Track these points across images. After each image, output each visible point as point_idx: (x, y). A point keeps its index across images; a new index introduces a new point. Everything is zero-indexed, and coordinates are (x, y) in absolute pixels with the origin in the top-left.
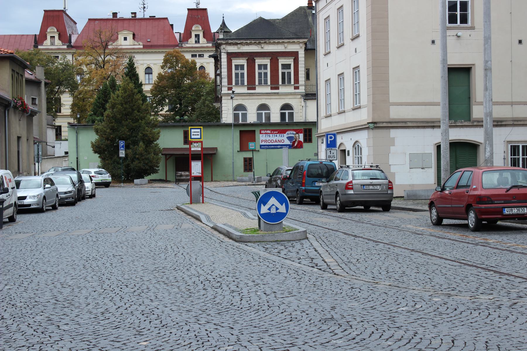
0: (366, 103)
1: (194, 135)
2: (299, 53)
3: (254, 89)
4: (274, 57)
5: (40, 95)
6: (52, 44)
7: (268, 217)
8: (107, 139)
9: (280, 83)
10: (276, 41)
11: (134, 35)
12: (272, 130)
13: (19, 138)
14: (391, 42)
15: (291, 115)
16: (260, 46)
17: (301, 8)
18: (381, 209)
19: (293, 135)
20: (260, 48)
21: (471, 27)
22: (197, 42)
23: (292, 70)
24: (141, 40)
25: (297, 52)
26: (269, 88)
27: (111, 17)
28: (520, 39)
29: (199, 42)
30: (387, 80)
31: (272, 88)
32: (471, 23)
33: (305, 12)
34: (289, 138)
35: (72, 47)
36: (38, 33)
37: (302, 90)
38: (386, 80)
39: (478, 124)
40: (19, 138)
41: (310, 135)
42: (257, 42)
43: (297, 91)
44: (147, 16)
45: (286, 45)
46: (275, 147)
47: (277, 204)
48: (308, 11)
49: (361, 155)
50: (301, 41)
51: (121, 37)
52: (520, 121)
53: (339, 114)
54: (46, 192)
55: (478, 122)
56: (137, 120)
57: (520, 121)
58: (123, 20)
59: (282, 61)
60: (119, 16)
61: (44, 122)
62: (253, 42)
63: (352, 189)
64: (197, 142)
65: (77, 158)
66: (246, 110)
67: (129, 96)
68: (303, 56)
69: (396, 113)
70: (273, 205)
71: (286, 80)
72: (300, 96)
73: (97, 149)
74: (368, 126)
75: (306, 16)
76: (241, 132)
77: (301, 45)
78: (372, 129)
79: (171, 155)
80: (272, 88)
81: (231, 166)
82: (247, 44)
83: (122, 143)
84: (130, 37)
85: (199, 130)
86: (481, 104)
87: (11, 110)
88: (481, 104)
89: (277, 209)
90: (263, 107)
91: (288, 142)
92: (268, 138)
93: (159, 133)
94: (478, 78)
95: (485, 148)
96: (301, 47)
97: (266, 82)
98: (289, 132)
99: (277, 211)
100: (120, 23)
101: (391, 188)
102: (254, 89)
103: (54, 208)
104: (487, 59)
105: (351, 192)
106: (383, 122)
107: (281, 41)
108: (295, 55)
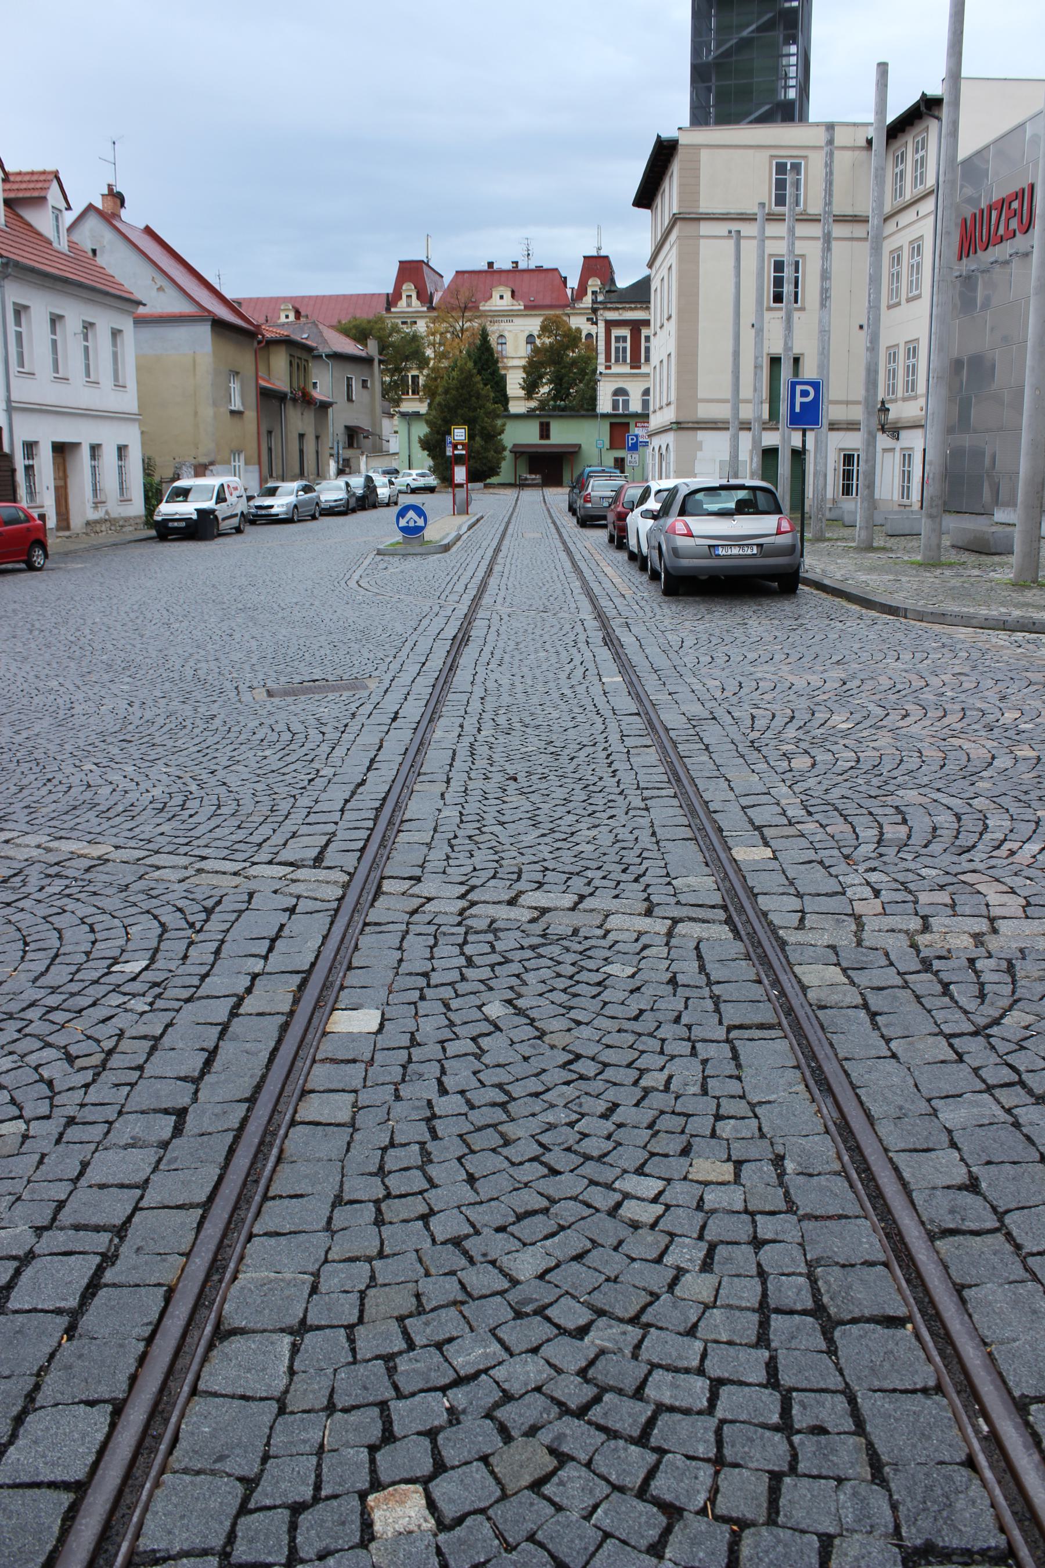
3: (639, 368)
5: (372, 375)
6: (409, 304)
7: (405, 530)
8: (438, 433)
11: (513, 292)
13: (301, 436)
14: (702, 325)
18: (170, 524)
24: (522, 299)
27: (486, 268)
35: (434, 309)
36: (390, 290)
38: (694, 372)
40: (301, 436)
44: (532, 266)
51: (496, 295)
54: (299, 501)
56: (475, 409)
58: (501, 272)
60: (496, 266)
61: (378, 410)
67: (466, 378)
73: (426, 444)
79: (523, 453)
82: (631, 309)
84: (508, 295)
87: (289, 405)
90: (620, 392)
93: (504, 425)
97: (625, 360)
100: (496, 276)
102: (639, 368)
103: (314, 518)
105: (589, 505)
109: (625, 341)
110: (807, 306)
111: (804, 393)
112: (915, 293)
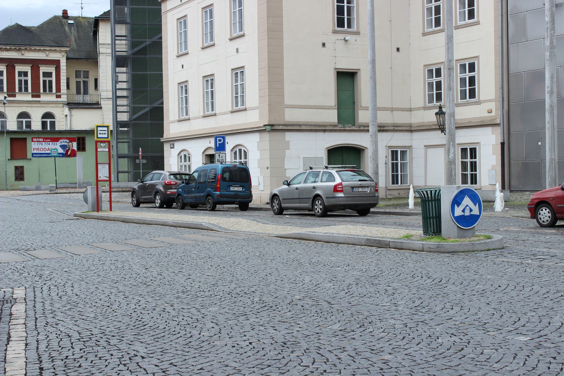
0: (256, 104)
1: (100, 134)
2: (61, 61)
4: (35, 64)
9: (42, 91)
10: (38, 48)
12: (44, 138)
14: (285, 42)
15: (53, 124)
16: (20, 53)
17: (56, 17)
19: (65, 144)
20: (20, 55)
21: (357, 32)
23: (54, 79)
25: (59, 61)
26: (30, 95)
28: (398, 47)
30: (282, 82)
31: (33, 96)
32: (357, 28)
33: (61, 22)
34: (63, 147)
37: (64, 98)
38: (281, 82)
39: (364, 129)
41: (84, 144)
42: (18, 48)
43: (59, 99)
45: (47, 53)
46: (48, 155)
47: (471, 204)
48: (64, 20)
50: (63, 49)
52: (400, 126)
53: (203, 117)
55: (364, 126)
57: (400, 126)
59: (43, 69)
62: (13, 48)
63: (341, 191)
64: (104, 142)
66: (30, 118)
68: (65, 64)
69: (291, 116)
70: (467, 206)
71: (48, 88)
72: (61, 105)
74: (264, 128)
75: (62, 25)
76: (12, 140)
77: (63, 54)
78: (269, 132)
80: (33, 96)
81: (4, 175)
82: (7, 50)
85: (99, 136)
86: (367, 109)
88: (367, 109)
89: (471, 210)
90: (23, 115)
91: (61, 151)
92: (40, 147)
94: (364, 84)
95: (449, 150)
96: (63, 56)
97: (26, 89)
98: (62, 140)
99: (472, 213)
101: (377, 191)
104: (450, 58)
105: (341, 195)
106: (279, 125)
107: (42, 48)
108: (56, 63)
109: (26, 74)
110: (361, 31)
111: (220, 140)
112: (184, 51)
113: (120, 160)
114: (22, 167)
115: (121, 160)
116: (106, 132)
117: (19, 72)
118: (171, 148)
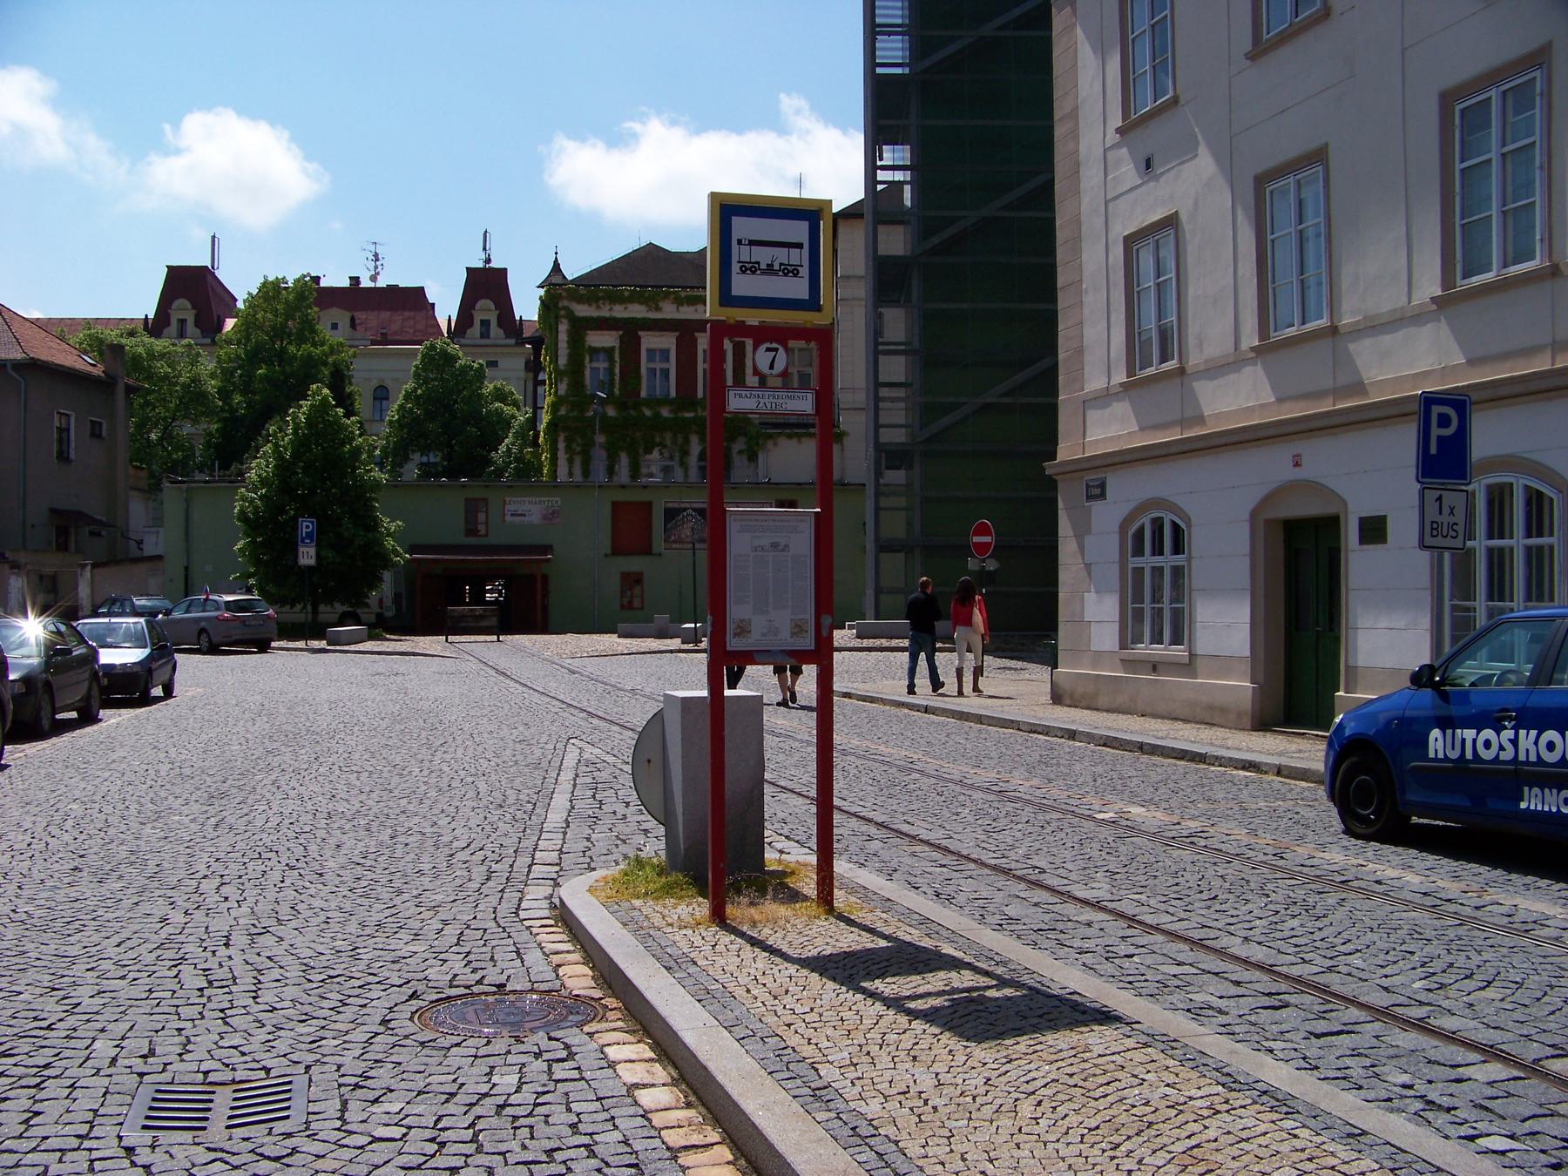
1: (750, 268)
22: (485, 334)
29: (488, 337)
49: (1178, 549)
65: (186, 568)
83: (306, 526)
85: (742, 285)
113: (885, 557)
114: (1363, 522)
115: (886, 558)
116: (800, 257)
117: (649, 351)
118: (1090, 498)
